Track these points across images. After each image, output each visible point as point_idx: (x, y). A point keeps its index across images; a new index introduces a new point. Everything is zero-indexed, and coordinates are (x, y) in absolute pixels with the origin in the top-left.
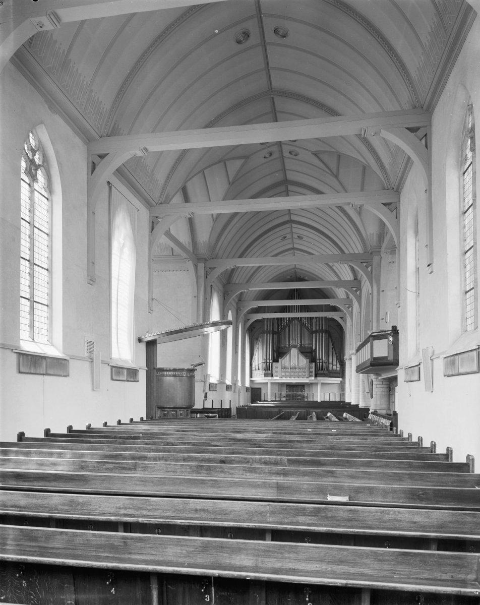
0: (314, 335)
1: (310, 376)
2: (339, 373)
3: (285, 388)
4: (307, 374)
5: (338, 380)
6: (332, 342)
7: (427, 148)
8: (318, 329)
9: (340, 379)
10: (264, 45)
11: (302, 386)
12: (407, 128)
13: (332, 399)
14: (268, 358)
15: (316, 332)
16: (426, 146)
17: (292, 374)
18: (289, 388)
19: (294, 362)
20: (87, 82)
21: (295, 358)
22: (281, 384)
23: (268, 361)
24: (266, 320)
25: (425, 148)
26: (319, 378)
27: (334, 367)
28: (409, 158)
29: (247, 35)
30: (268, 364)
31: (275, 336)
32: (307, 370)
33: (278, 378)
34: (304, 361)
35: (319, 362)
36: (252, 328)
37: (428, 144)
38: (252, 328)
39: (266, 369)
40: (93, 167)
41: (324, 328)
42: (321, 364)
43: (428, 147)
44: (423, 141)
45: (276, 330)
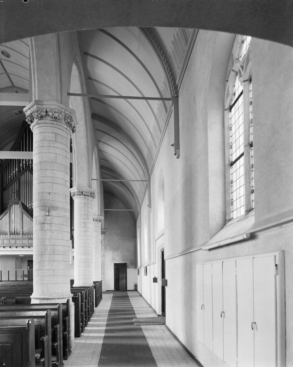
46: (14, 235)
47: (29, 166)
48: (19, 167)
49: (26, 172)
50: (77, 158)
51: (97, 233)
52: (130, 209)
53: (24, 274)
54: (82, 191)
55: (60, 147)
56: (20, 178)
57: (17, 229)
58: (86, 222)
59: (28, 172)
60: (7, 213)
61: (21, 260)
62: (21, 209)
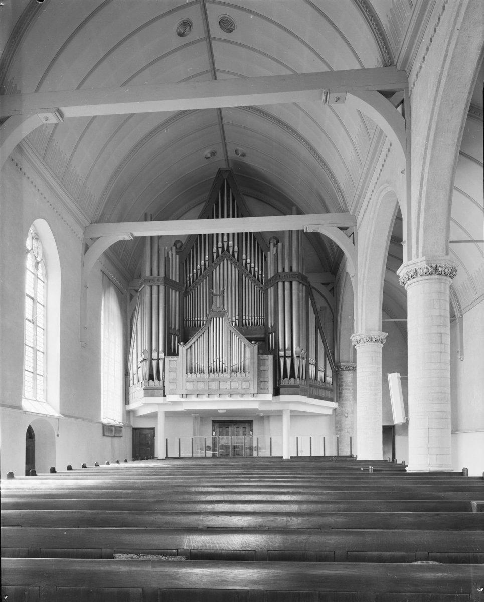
0: (271, 292)
1: (261, 389)
2: (332, 391)
3: (209, 428)
4: (253, 386)
5: (326, 407)
6: (316, 312)
7: (354, 244)
8: (280, 270)
9: (334, 405)
10: (209, 38)
11: (240, 422)
12: (380, 92)
13: (318, 452)
14: (154, 348)
15: (273, 282)
16: (403, 115)
17: (214, 385)
18: (220, 427)
19: (220, 355)
20: (67, 159)
21: (221, 342)
22: (201, 416)
23: (155, 355)
24: (149, 242)
25: (353, 244)
26: (283, 398)
27: (321, 375)
28: (381, 132)
29: (187, 24)
30: (155, 363)
31: (175, 296)
32: (252, 375)
33: (177, 398)
34: (244, 351)
35: (285, 357)
36: (133, 293)
37: (355, 242)
38: (133, 293)
39: (151, 377)
40: (87, 248)
41: (295, 269)
42: (289, 361)
43: (406, 116)
44: (400, 109)
45: (175, 277)
46: (215, 373)
47: (228, 250)
48: (211, 253)
49: (223, 261)
50: (427, 194)
51: (377, 366)
52: (396, 318)
53: (207, 445)
54: (437, 266)
55: (403, 172)
56: (213, 272)
57: (224, 365)
58: (442, 332)
59: (227, 260)
60: (203, 333)
61: (200, 420)
62: (227, 323)
